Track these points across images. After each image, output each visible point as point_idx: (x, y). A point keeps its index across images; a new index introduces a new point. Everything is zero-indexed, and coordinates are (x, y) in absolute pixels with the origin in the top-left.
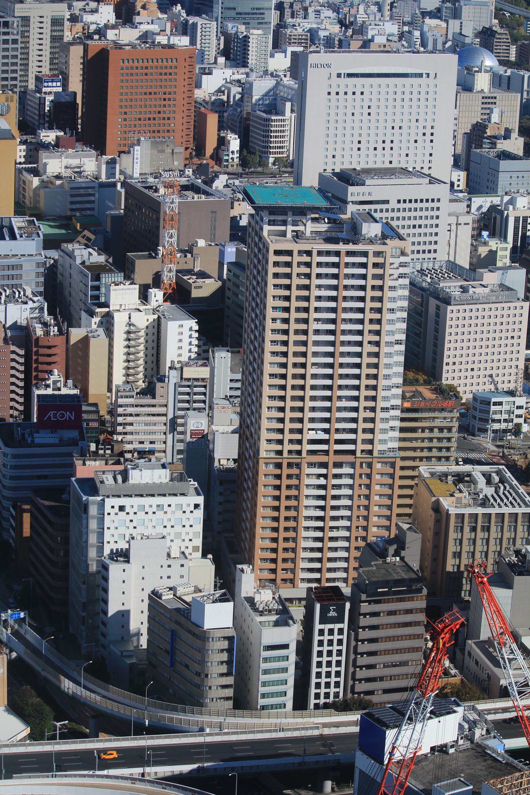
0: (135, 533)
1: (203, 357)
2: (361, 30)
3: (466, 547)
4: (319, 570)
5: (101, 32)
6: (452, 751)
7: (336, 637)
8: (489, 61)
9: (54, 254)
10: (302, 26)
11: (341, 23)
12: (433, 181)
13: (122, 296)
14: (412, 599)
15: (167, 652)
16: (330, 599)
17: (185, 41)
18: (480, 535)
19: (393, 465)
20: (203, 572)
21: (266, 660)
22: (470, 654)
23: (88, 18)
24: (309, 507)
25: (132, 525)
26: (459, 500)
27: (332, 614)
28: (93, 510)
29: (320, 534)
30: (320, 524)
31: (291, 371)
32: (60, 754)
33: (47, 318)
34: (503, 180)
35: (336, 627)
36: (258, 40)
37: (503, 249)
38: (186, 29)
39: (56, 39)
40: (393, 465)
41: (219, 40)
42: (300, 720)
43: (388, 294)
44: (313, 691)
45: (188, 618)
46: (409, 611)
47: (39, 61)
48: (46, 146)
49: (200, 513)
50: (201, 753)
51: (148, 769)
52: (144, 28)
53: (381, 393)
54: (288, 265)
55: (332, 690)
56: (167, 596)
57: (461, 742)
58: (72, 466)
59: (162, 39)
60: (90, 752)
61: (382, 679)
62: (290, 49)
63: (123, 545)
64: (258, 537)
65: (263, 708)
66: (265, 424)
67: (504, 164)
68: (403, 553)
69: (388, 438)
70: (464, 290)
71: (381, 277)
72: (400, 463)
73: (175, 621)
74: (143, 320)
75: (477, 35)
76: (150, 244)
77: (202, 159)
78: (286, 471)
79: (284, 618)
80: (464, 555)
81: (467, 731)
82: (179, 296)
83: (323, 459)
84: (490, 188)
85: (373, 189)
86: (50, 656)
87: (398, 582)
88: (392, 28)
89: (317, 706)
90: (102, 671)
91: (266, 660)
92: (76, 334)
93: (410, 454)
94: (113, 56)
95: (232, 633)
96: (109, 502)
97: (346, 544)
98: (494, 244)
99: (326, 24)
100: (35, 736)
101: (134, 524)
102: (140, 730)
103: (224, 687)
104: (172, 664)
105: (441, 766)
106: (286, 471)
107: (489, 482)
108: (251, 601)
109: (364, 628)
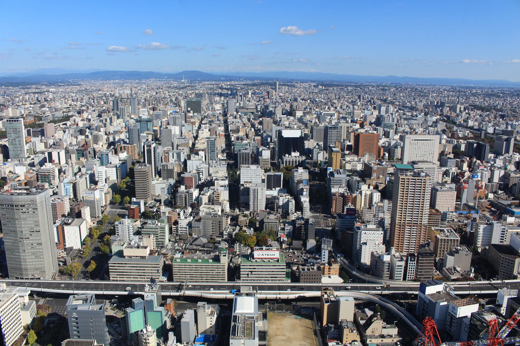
1: (382, 201)
2: (414, 130)
3: (443, 246)
5: (357, 130)
8: (445, 137)
9: (349, 178)
10: (401, 129)
11: (410, 128)
12: (434, 164)
13: (364, 187)
17: (375, 132)
18: (446, 244)
19: (426, 227)
20: (383, 248)
23: (354, 127)
24: (406, 235)
28: (359, 233)
31: (404, 205)
33: (348, 192)
34: (449, 164)
36: (392, 132)
37: (448, 179)
38: (376, 130)
39: (348, 131)
40: (426, 227)
43: (427, 189)
44: (407, 276)
47: (344, 136)
48: (346, 155)
49: (382, 235)
52: (366, 129)
53: (424, 211)
54: (404, 181)
56: (375, 253)
58: (354, 223)
59: (370, 132)
62: (399, 134)
66: (398, 216)
67: (449, 160)
69: (425, 221)
70: (441, 188)
71: (425, 185)
72: (428, 227)
73: (376, 260)
74: (369, 193)
75: (441, 131)
76: (370, 176)
77: (380, 158)
78: (402, 227)
79: (402, 260)
82: (376, 187)
83: (410, 224)
84: (445, 166)
85: (420, 165)
88: (422, 129)
92: (354, 195)
93: (430, 224)
94: (361, 135)
96: (363, 232)
98: (447, 178)
99: (406, 129)
100: (344, 282)
102: (369, 282)
105: (439, 296)
106: (402, 227)
107: (448, 232)
108: (394, 255)
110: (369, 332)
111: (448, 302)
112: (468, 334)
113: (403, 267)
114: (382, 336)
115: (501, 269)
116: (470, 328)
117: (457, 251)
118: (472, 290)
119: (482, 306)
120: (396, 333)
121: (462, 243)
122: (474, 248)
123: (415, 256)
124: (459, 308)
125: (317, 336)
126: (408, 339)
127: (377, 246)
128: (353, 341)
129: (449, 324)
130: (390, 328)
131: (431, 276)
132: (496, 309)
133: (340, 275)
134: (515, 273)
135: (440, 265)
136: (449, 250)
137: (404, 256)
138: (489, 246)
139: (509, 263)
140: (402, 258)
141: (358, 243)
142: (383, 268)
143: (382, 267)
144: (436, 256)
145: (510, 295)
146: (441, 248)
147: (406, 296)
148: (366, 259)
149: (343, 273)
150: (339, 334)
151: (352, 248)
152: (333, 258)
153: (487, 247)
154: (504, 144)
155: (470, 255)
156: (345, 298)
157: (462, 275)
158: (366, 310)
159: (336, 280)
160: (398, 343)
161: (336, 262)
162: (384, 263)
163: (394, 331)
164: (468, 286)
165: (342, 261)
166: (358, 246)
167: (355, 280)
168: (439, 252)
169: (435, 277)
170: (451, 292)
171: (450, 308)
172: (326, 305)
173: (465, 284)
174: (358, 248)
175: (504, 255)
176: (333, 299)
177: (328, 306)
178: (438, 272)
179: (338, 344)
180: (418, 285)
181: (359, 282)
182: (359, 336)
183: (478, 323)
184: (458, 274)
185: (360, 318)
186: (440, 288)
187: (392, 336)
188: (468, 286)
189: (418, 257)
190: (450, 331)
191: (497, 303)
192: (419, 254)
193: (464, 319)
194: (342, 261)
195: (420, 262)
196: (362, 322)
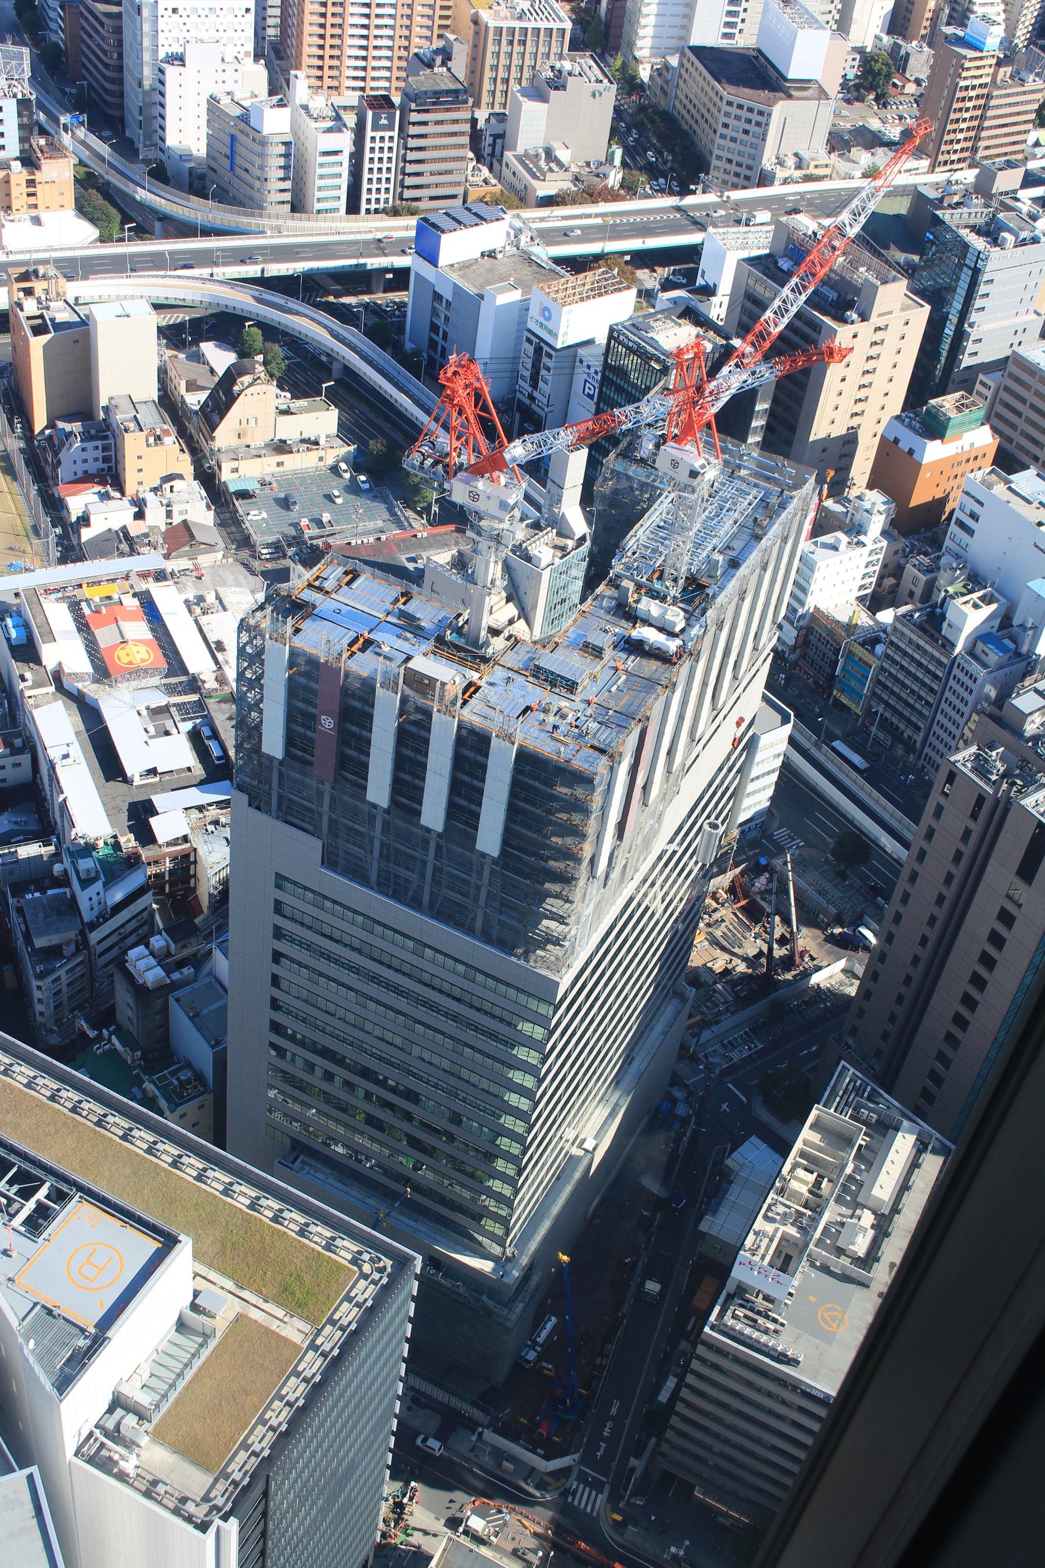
0: (188, 36)
3: (503, 61)
4: (363, 79)
6: (500, 256)
7: (387, 144)
14: (458, 109)
15: (227, 156)
16: (381, 107)
18: (517, 48)
20: (256, 76)
21: (321, 165)
22: (507, 165)
25: (185, 28)
26: (497, 13)
27: (384, 122)
29: (364, 43)
30: (365, 32)
32: (132, 256)
35: (387, 134)
42: (354, 224)
44: (365, 196)
45: (248, 123)
46: (456, 122)
51: (216, 270)
55: (383, 196)
56: (225, 101)
57: (508, 248)
60: (161, 254)
61: (428, 186)
63: (177, 49)
64: (305, 44)
65: (319, 212)
68: (450, 64)
73: (234, 132)
79: (338, 125)
80: (501, 69)
87: (448, 92)
89: (368, 211)
90: (161, 173)
91: (321, 165)
95: (288, 138)
97: (389, 54)
100: (103, 240)
101: (187, 27)
102: (207, 232)
103: (282, 191)
104: (232, 169)
105: (491, 270)
108: (305, 108)
109: (413, 137)
110: (225, 435)
111: (526, 288)
112: (598, 404)
113: (345, 158)
114: (281, 447)
115: (720, 150)
116: (602, 384)
117: (558, 82)
118: (612, 238)
119: (646, 295)
120: (334, 429)
121: (576, 45)
122: (624, 65)
123: (391, 105)
124: (565, 309)
125: (15, 478)
126: (376, 446)
127: (230, 69)
129: (527, 374)
131: (459, 191)
132: (695, 301)
133: (82, 209)
134: (767, 162)
135: (489, 145)
136: (526, 74)
137: (345, 108)
138: (683, 55)
139: (749, 121)
140: (338, 118)
141: (147, 57)
142: (262, 168)
143: (258, 161)
144: (477, 104)
145: (744, 248)
146: (495, 68)
147: (358, 279)
148: (186, 133)
149: (95, 195)
150: (105, 460)
151: (121, 82)
152: (43, 132)
153: (674, 61)
154: (549, 1326)
155: (610, 93)
156: (115, 308)
157: (576, 179)
158: (208, 348)
159: (70, 232)
160: (343, 466)
161: (55, 150)
162: (263, 143)
165: (83, 143)
166: (147, 72)
167: (143, 223)
168: (487, 86)
169: (474, 194)
171: (534, 312)
172: (37, 345)
173: (589, 216)
174: (147, 84)
175: (732, 89)
176: (64, 316)
177: (46, 347)
178: (485, 172)
179: (105, 497)
181: (167, 235)
182: (187, 457)
183: (631, 362)
184: (561, 174)
185: (183, 384)
186: (492, 235)
187: (316, 443)
188: (599, 221)
189: (405, 111)
190: (531, 397)
191: (700, 281)
192: (407, 96)
193: (582, 352)
194: (83, 143)
195: (413, 130)
196: (195, 400)
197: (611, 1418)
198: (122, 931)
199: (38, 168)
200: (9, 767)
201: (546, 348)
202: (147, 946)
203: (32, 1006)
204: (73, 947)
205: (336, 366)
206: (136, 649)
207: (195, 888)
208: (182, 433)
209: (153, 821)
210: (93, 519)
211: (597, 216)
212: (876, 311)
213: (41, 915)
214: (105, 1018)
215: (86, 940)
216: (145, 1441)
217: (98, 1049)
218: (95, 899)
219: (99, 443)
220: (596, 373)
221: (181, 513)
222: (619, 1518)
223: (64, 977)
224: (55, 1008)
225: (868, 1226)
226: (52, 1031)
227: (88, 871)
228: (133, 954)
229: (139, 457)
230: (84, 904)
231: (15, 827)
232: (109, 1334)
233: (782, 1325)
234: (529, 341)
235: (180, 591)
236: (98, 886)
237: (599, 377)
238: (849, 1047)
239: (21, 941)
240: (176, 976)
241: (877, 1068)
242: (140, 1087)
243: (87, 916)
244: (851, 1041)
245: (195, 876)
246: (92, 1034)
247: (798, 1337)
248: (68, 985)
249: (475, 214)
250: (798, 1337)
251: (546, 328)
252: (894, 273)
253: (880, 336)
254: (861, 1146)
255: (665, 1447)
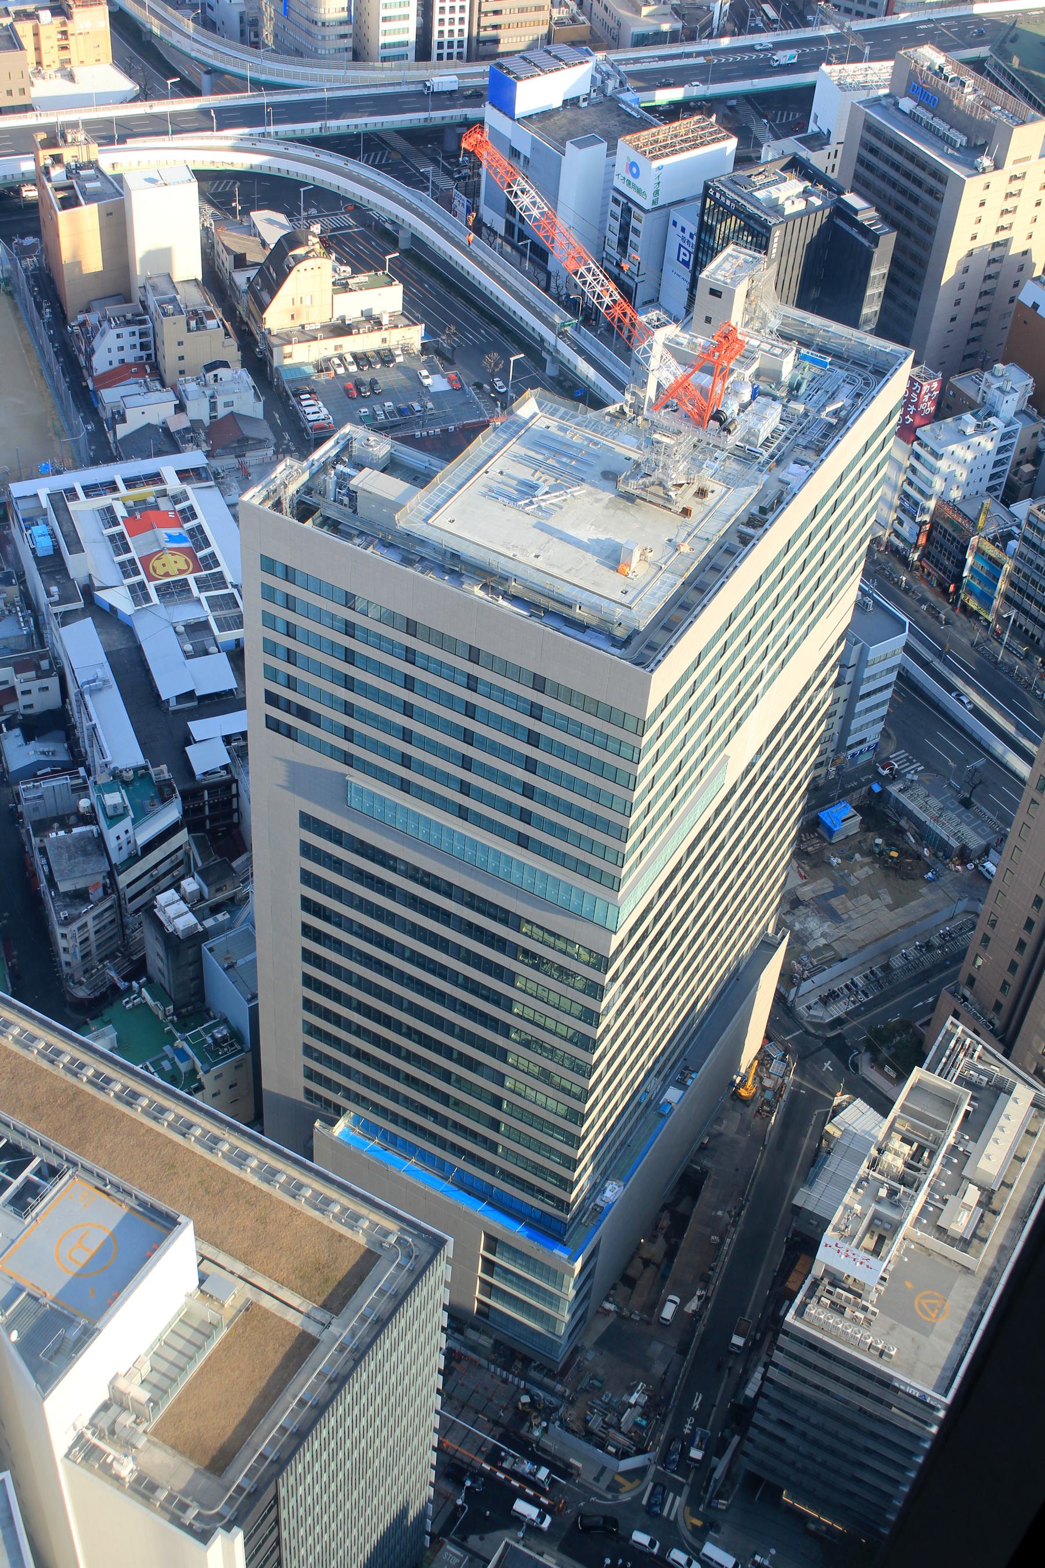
32: (175, 115)
41: (838, 644)
50: (323, 110)
57: (593, 95)
81: (598, 84)
86: (199, 38)
103: (344, 36)
105: (573, 122)
110: (276, 317)
114: (342, 329)
128: (210, 367)
129: (615, 239)
130: (368, 286)
133: (123, 63)
163: (389, 298)
164: (701, 60)
170: (627, 97)
173: (689, 55)
180: (482, 75)
182: (233, 342)
188: (701, 60)
191: (812, 128)
197: (694, 1414)
198: (155, 872)
199: (69, 17)
200: (35, 691)
201: (634, 209)
202: (178, 889)
203: (58, 955)
204: (100, 891)
205: (401, 235)
206: (172, 558)
207: (238, 824)
208: (230, 313)
209: (188, 749)
210: (128, 413)
211: (699, 54)
212: (1012, 155)
213: (65, 856)
214: (138, 969)
215: (114, 883)
216: (142, 1442)
217: (128, 1003)
218: (123, 837)
219: (136, 328)
220: (691, 236)
221: (227, 405)
222: (698, 1523)
223: (91, 924)
224: (83, 957)
225: (973, 1203)
226: (81, 983)
227: (115, 807)
228: (162, 899)
229: (180, 343)
230: (112, 844)
231: (43, 758)
232: (98, 1325)
233: (874, 1314)
234: (616, 201)
235: (223, 494)
236: (126, 823)
237: (694, 241)
238: (965, 999)
239: (43, 885)
240: (209, 923)
241: (997, 1022)
242: (172, 1046)
243: (117, 858)
244: (967, 993)
245: (237, 810)
246: (122, 985)
247: (892, 1328)
248: (96, 932)
249: (555, 57)
250: (892, 1328)
251: (634, 187)
252: (1032, 112)
253: (1016, 186)
254: (967, 1112)
255: (748, 1447)
